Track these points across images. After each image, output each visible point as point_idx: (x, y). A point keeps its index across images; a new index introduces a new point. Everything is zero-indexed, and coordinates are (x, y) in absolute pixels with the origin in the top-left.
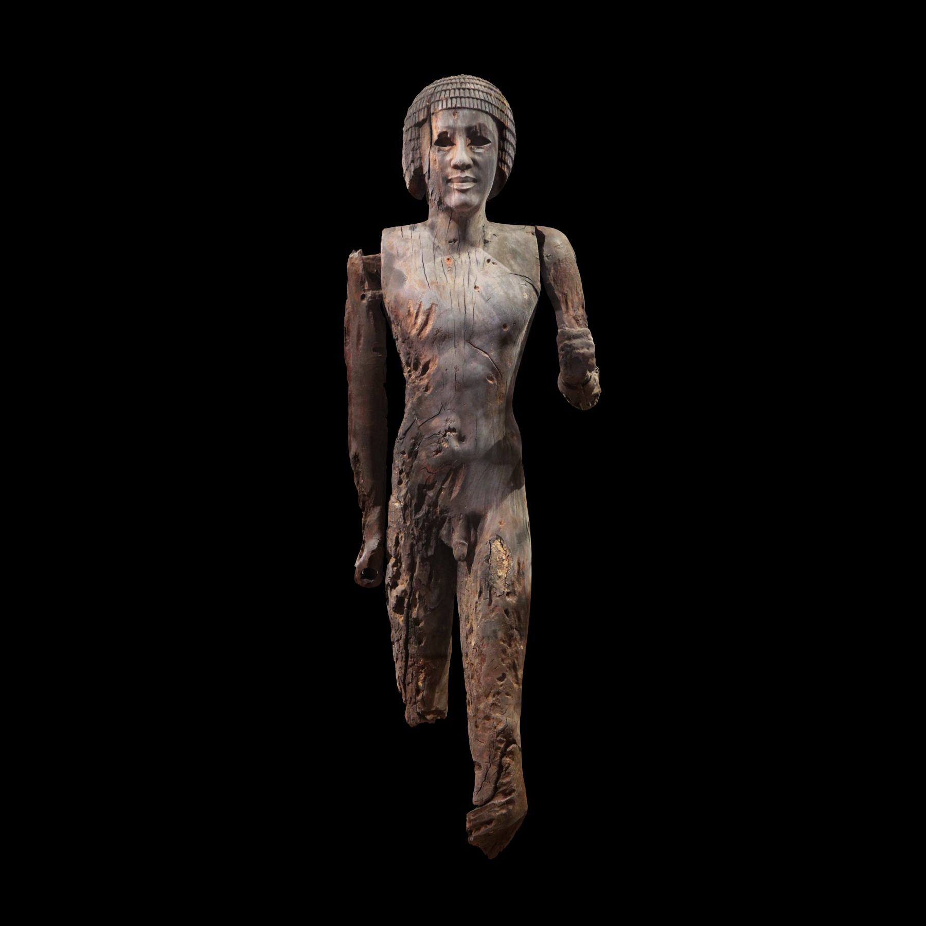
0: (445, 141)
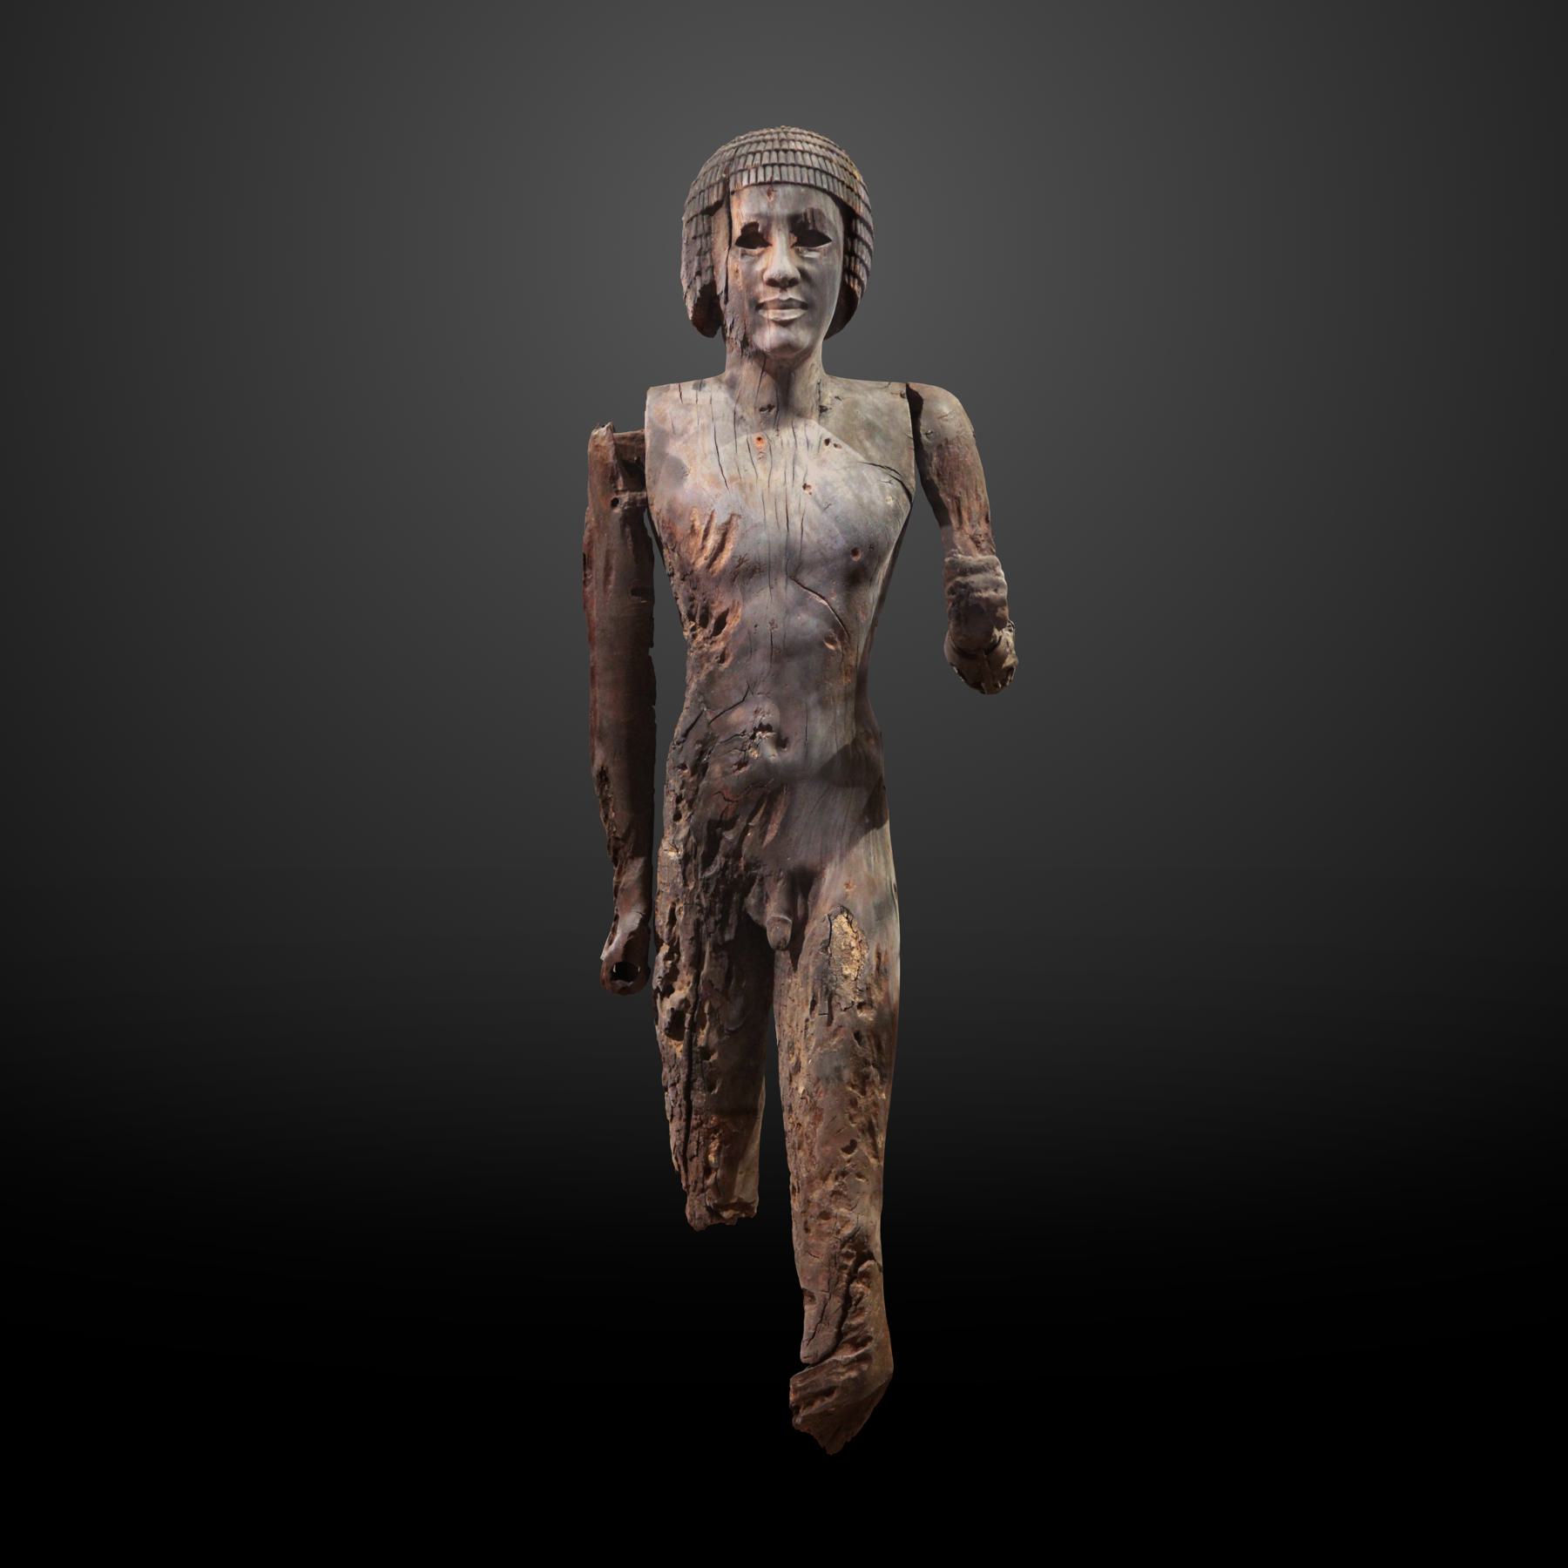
0: (754, 238)
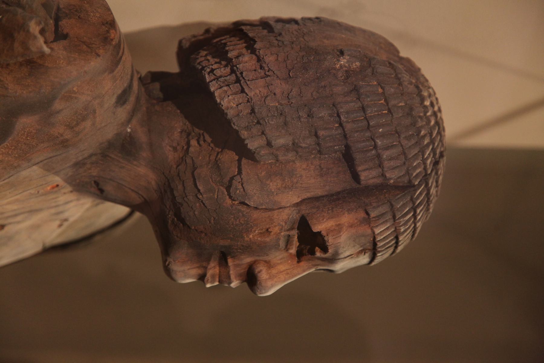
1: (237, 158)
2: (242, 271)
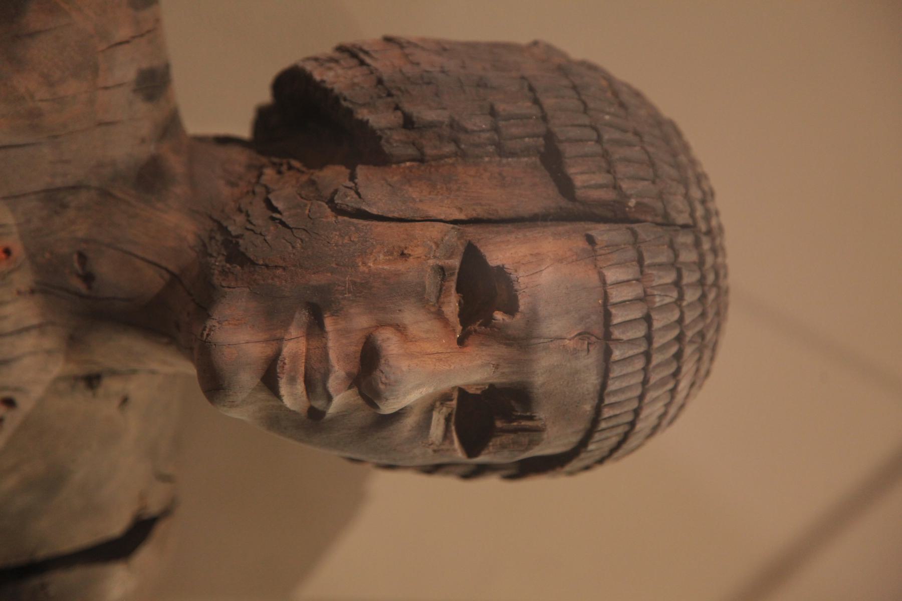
0: (480, 299)
1: (348, 171)
2: (352, 349)
